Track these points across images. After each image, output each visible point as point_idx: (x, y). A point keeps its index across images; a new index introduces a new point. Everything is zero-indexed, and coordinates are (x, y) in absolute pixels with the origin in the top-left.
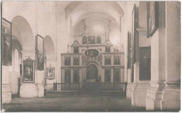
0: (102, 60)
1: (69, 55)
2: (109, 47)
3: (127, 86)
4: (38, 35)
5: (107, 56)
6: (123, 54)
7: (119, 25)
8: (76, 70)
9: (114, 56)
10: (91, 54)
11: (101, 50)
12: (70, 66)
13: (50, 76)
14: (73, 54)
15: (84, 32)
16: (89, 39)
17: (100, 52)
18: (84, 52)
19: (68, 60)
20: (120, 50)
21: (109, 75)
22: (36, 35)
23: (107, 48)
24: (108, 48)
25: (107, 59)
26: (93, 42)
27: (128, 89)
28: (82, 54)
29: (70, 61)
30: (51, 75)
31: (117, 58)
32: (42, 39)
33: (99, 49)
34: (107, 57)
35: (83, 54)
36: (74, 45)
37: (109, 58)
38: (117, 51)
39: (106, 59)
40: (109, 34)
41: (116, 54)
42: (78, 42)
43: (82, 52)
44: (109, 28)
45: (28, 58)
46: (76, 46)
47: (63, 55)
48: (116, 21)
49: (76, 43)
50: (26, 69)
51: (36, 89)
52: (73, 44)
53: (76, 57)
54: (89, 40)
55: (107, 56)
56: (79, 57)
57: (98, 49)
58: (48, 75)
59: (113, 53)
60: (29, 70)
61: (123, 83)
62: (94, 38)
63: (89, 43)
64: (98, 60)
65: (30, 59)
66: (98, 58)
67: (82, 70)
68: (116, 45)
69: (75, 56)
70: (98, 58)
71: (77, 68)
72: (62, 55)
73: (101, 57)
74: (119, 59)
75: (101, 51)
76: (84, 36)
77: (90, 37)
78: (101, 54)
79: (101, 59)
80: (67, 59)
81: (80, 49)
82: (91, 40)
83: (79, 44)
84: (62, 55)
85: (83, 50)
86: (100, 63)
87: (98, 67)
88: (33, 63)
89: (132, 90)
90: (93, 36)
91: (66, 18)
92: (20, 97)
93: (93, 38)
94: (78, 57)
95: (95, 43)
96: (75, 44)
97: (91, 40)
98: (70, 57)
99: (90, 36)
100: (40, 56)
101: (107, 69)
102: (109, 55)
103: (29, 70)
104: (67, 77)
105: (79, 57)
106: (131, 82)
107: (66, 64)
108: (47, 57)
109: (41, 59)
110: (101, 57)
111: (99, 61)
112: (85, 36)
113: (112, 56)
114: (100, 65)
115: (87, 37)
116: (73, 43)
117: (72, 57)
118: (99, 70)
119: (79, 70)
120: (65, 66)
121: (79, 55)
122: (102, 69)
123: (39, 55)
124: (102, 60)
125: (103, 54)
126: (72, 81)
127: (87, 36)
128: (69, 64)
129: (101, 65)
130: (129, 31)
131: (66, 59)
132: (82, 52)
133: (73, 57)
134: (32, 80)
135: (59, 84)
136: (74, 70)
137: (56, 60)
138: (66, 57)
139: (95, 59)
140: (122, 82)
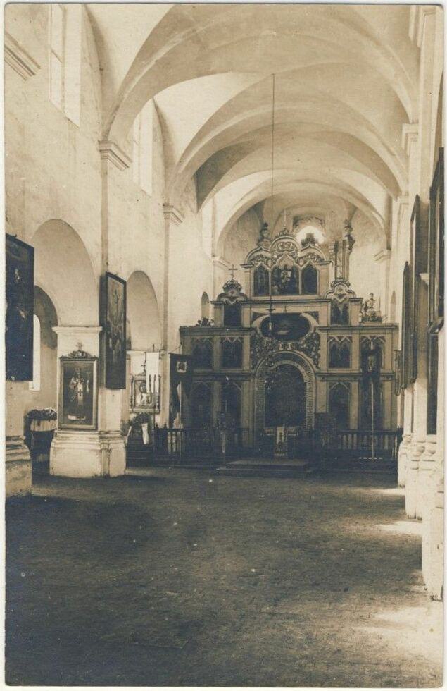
2: (346, 307)
14: (221, 330)
17: (313, 322)
25: (337, 346)
26: (289, 288)
33: (309, 313)
35: (256, 332)
36: (224, 299)
40: (350, 253)
42: (240, 289)
44: (346, 233)
45: (76, 349)
46: (232, 303)
52: (221, 296)
54: (277, 281)
55: (338, 337)
56: (239, 340)
57: (306, 312)
58: (138, 401)
60: (80, 387)
63: (276, 291)
64: (305, 351)
65: (83, 353)
68: (372, 294)
73: (315, 342)
75: (318, 321)
76: (261, 267)
81: (246, 313)
83: (242, 295)
85: (256, 316)
88: (92, 364)
93: (289, 274)
94: (237, 341)
95: (295, 292)
98: (211, 339)
99: (281, 267)
101: (337, 383)
103: (80, 387)
111: (308, 355)
114: (314, 366)
117: (217, 339)
122: (318, 382)
125: (322, 329)
127: (268, 268)
129: (318, 368)
132: (252, 322)
134: (89, 421)
139: (297, 347)
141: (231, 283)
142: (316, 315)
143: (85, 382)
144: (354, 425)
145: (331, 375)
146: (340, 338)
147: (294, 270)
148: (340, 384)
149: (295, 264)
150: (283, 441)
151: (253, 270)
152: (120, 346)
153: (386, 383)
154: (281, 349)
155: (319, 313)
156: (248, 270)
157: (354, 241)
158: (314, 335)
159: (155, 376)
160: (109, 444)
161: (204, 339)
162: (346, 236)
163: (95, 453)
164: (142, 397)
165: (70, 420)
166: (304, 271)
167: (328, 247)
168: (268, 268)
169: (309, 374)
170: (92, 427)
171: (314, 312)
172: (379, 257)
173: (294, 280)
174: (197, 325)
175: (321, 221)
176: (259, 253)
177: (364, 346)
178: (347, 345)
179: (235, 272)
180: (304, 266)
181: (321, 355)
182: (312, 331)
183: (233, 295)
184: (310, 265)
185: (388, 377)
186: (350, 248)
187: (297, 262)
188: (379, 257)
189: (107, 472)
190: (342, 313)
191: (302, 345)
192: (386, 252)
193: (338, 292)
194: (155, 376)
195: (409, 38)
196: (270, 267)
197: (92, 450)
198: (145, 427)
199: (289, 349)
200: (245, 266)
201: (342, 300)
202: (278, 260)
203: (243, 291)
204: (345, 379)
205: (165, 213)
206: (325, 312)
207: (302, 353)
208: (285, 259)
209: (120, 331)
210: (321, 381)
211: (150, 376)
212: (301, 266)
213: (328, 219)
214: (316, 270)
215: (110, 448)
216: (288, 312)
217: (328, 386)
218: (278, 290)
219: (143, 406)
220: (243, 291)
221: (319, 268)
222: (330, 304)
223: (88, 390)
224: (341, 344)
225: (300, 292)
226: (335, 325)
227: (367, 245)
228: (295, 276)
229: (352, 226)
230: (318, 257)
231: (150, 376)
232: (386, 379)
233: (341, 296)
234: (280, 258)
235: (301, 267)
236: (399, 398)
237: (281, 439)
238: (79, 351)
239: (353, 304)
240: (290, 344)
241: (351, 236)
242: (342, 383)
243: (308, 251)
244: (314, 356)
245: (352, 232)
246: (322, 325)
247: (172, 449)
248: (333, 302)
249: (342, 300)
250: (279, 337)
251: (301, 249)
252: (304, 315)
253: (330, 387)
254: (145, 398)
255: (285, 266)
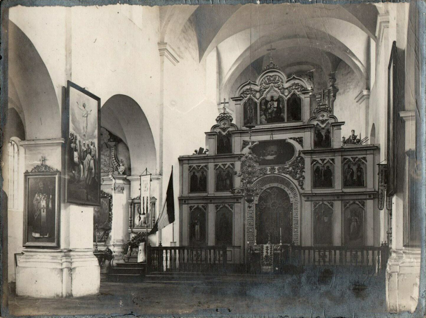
0: (304, 174)
1: (202, 161)
2: (328, 132)
3: (390, 263)
4: (70, 84)
5: (321, 159)
6: (375, 152)
7: (362, 69)
8: (225, 206)
9: (345, 159)
10: (269, 155)
11: (300, 141)
12: (204, 194)
13: (141, 226)
14: (214, 158)
15: (248, 87)
16: (263, 107)
17: (298, 147)
18: (246, 151)
19: (199, 175)
20: (366, 138)
21: (326, 220)
22: (65, 84)
23: (321, 135)
24: (323, 133)
25: (321, 168)
27: (390, 275)
28: (239, 157)
29: (204, 180)
30: (145, 223)
31: (355, 164)
32: (95, 102)
33: (294, 139)
34: (320, 162)
36: (218, 130)
37: (328, 167)
38: (354, 143)
39: (318, 168)
40: (333, 101)
41: (348, 153)
42: (231, 120)
43: (242, 150)
44: (331, 83)
45: (39, 163)
46: (224, 134)
47: (184, 162)
48: (354, 55)
49: (225, 124)
50: (35, 202)
51: (62, 270)
52: (214, 127)
53: (222, 167)
54: (265, 111)
55: (321, 159)
56: (231, 166)
57: (291, 138)
58: (137, 222)
59: (341, 151)
61: (373, 248)
62: (278, 105)
63: (264, 120)
64: (290, 173)
66: (291, 169)
67: (242, 206)
68: (354, 131)
69: (220, 164)
70: (291, 169)
71: (227, 201)
72: (181, 160)
73: (300, 165)
74: (360, 169)
75: (302, 146)
76: (250, 99)
77: (268, 101)
78: (302, 155)
79: (302, 171)
80: (198, 172)
81: (237, 142)
82: (270, 111)
83: (232, 125)
84: (181, 160)
85: (245, 144)
86: (296, 182)
87: (291, 196)
88: (55, 178)
89: (413, 296)
90: (275, 98)
91: (201, 55)
92: (17, 296)
93: (276, 104)
94: (229, 167)
95: (282, 120)
96: (222, 126)
97: (270, 111)
98: (206, 166)
99: (268, 98)
100: (82, 158)
101: (321, 203)
102: (328, 158)
104: (197, 227)
105: (231, 166)
106: (404, 248)
107: (193, 189)
108: (132, 167)
109: (87, 167)
110: (300, 165)
111: (293, 177)
112: (252, 100)
113: (338, 160)
114: (299, 187)
115: (258, 101)
116: (215, 123)
117: (211, 166)
118: (294, 206)
119: (232, 208)
120: (191, 195)
121: (233, 160)
122: (303, 202)
123: (76, 154)
124: (304, 174)
125: (306, 153)
126: (211, 240)
127: (256, 100)
128: (204, 189)
129: (303, 189)
130: (397, 45)
131: (194, 173)
132: (242, 150)
133: (216, 166)
134: (51, 239)
135: (166, 248)
136: (217, 207)
137: (160, 177)
138: (194, 168)
139: (284, 170)
140: (370, 242)
141: (223, 115)
142: (300, 141)
143: (49, 198)
144: (337, 241)
145: (316, 195)
146: (323, 160)
147: (279, 100)
148: (323, 203)
149: (281, 94)
150: (269, 254)
151: (242, 102)
152: (92, 162)
153: (368, 201)
154: (269, 173)
155: (303, 139)
156: (239, 102)
157: (338, 90)
158: (299, 159)
159: (147, 197)
160: (71, 263)
161: (200, 166)
162: (331, 86)
163: (56, 273)
164: (140, 218)
165: (35, 237)
166: (289, 99)
167: (315, 96)
168: (256, 100)
169: (295, 195)
170: (54, 244)
171: (298, 138)
172: (361, 98)
173: (279, 110)
174: (194, 154)
175: (310, 76)
176: (248, 87)
177: (346, 166)
178: (331, 168)
179: (227, 105)
180: (289, 96)
181: (191, 6)
182: (297, 155)
183: (226, 126)
184: (294, 94)
185: (370, 195)
186: (334, 96)
187: (283, 93)
188: (361, 98)
189: (70, 292)
190: (324, 137)
191: (288, 168)
192: (365, 92)
193: (321, 118)
194: (147, 197)
195: (376, 2)
196: (258, 99)
197: (54, 269)
198: (141, 247)
199: (276, 172)
200: (235, 99)
201: (325, 125)
202: (265, 92)
203: (234, 122)
204: (329, 198)
205: (160, 50)
206: (308, 137)
207: (288, 176)
208: (272, 91)
209: (92, 147)
210: (306, 201)
211: (144, 197)
212: (286, 96)
213: (316, 75)
214: (300, 99)
215: (73, 267)
216: (274, 139)
217: (313, 205)
218: (266, 120)
219: (141, 227)
220: (234, 122)
221: (302, 96)
222: (313, 130)
223: (50, 206)
224: (324, 167)
225: (286, 120)
226: (318, 149)
227: (348, 92)
228: (281, 106)
229: (336, 78)
230: (302, 87)
231: (144, 197)
232: (368, 197)
233: (323, 122)
234: (267, 90)
235: (286, 96)
236: (383, 213)
237: (267, 252)
238: (42, 164)
239: (335, 128)
240: (276, 168)
241: (335, 86)
242: (325, 203)
243: (292, 82)
244: (300, 177)
245: (336, 83)
246: (305, 149)
247: (167, 266)
248: (315, 127)
249: (325, 125)
250: (268, 162)
251: (286, 80)
252: (292, 141)
253: (315, 206)
254: (142, 219)
255: (272, 97)
